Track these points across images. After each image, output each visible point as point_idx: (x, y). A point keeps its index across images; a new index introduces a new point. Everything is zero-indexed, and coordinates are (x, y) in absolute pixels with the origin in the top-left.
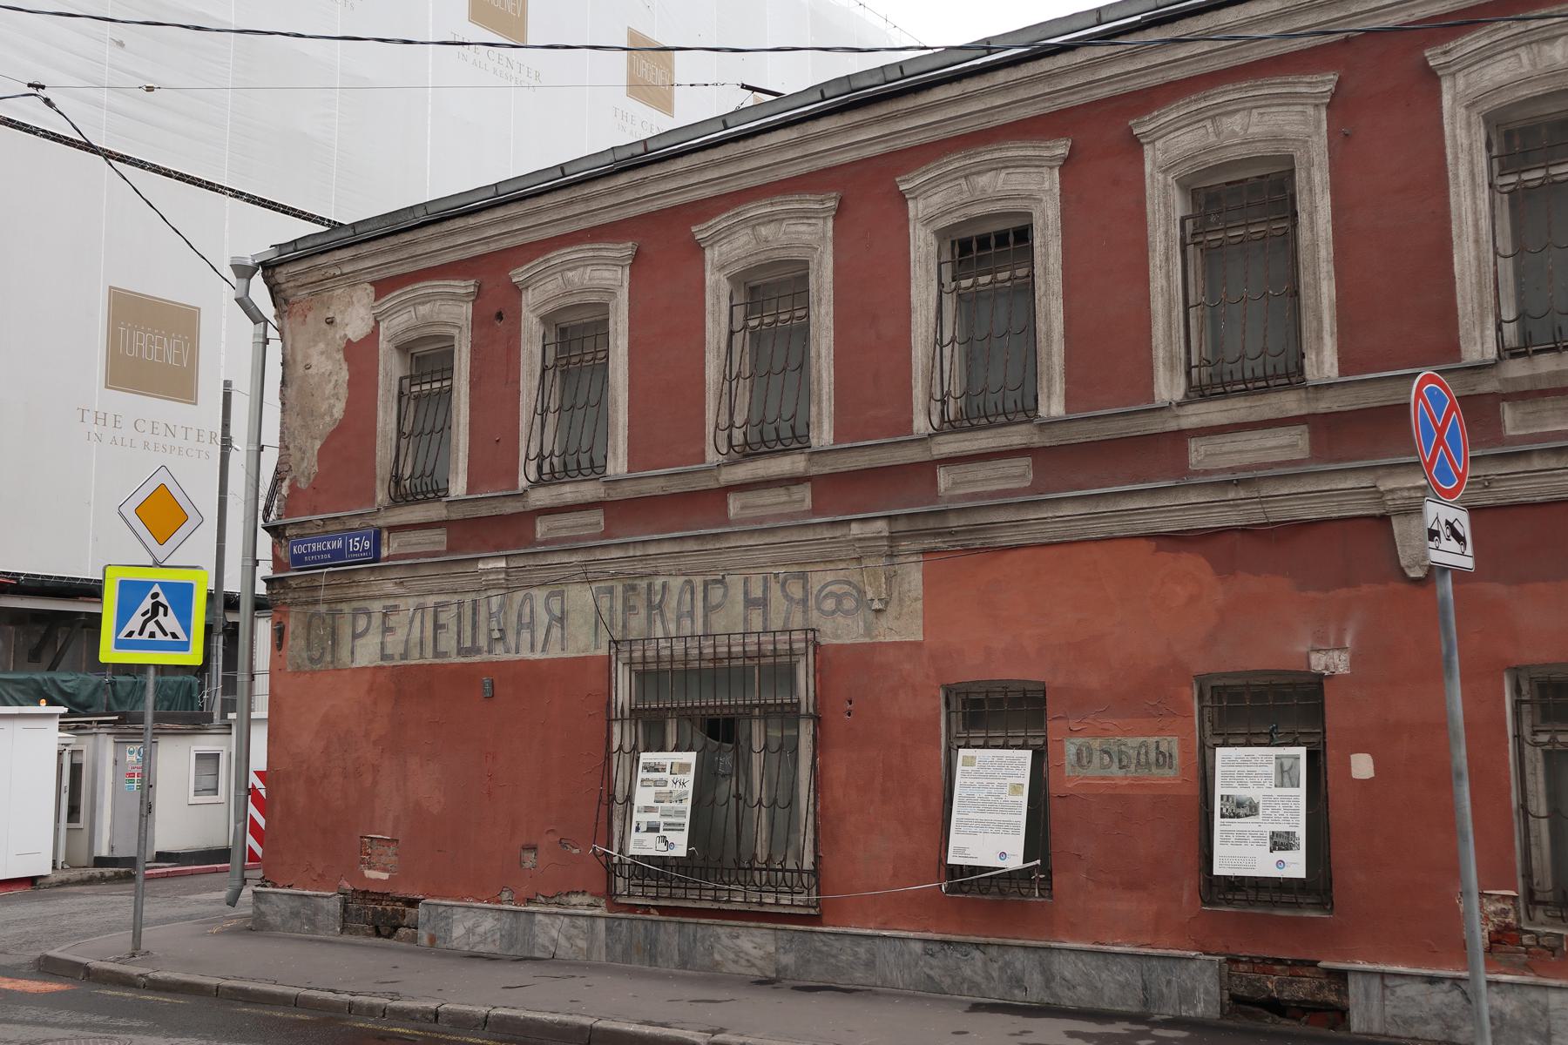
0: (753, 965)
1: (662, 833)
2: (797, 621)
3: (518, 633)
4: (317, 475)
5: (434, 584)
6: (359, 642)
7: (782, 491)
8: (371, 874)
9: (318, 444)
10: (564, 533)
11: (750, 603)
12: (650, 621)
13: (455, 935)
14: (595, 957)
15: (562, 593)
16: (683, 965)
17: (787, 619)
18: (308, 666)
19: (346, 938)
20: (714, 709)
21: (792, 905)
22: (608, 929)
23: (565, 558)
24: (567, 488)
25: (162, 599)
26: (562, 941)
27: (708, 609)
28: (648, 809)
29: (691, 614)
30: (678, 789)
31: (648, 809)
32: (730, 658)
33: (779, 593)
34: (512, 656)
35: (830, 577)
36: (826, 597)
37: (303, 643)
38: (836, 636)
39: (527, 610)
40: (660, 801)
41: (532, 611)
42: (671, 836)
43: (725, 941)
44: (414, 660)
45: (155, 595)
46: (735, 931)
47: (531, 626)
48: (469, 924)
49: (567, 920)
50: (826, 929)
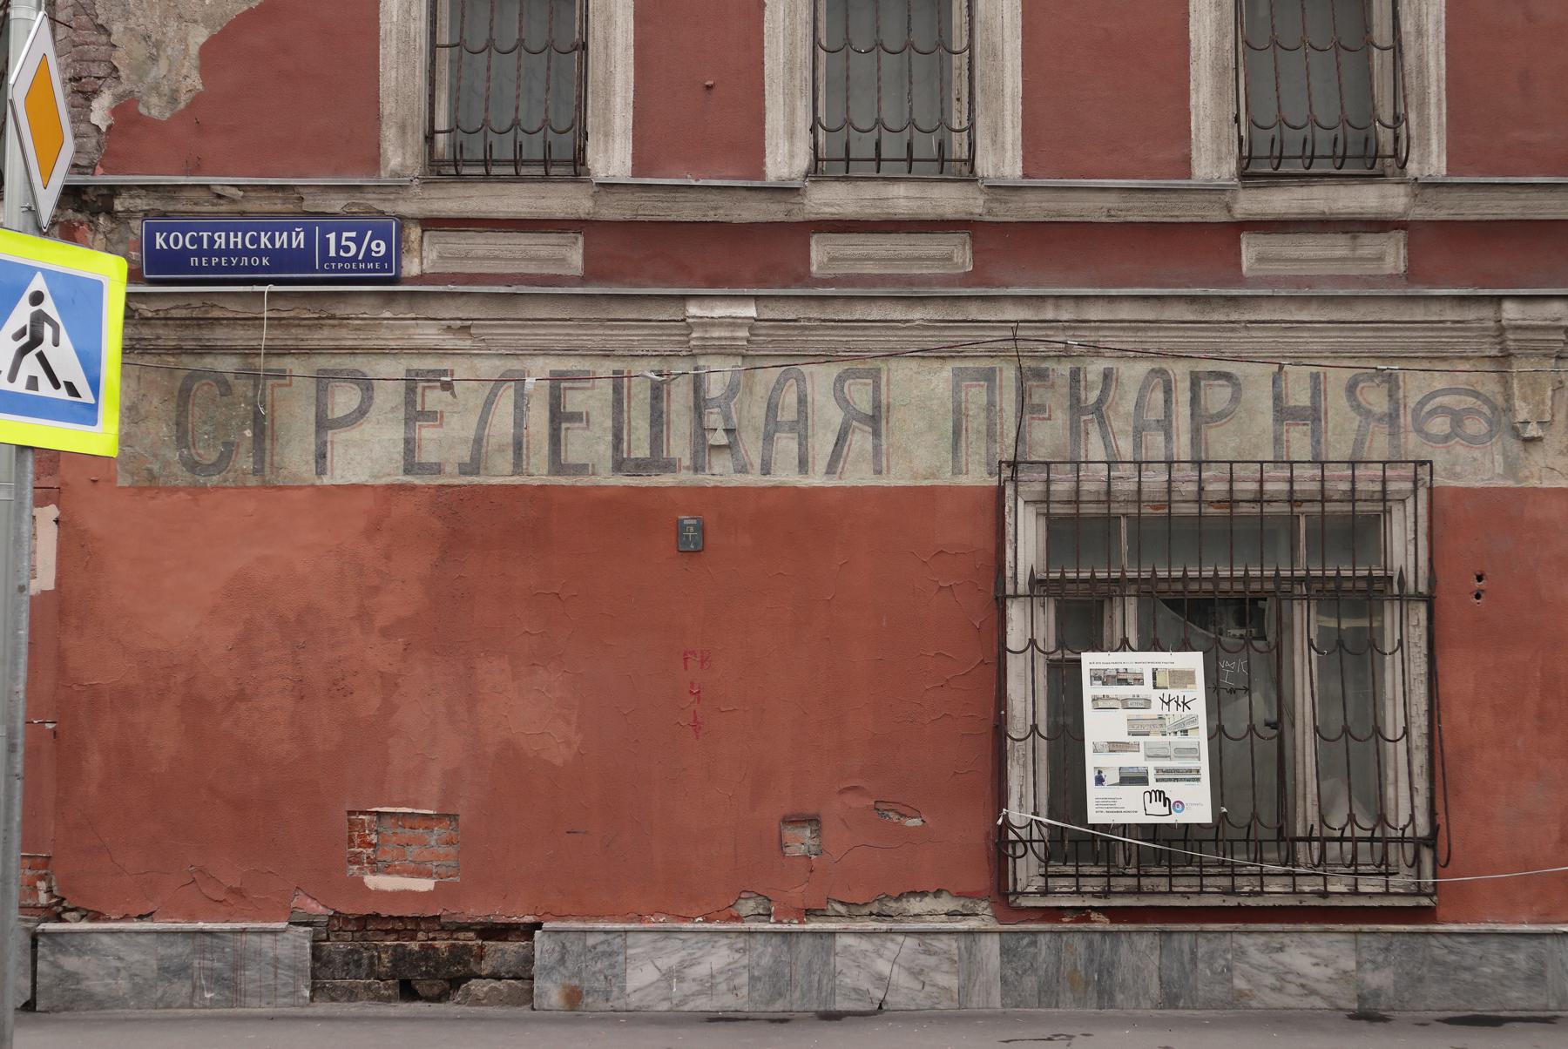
0: (1313, 992)
1: (1153, 785)
2: (1379, 446)
3: (768, 438)
4: (197, 100)
5: (543, 336)
6: (337, 437)
7: (1342, 239)
8: (374, 881)
9: (199, 36)
10: (870, 269)
11: (1283, 413)
12: (1076, 432)
13: (631, 985)
14: (976, 1002)
15: (875, 375)
16: (1170, 1000)
17: (1359, 443)
18: (183, 477)
19: (322, 1008)
20: (1224, 580)
21: (1387, 893)
22: (1005, 951)
23: (897, 313)
24: (900, 190)
25: (48, 307)
26: (901, 979)
27: (1199, 420)
28: (1115, 747)
29: (1166, 426)
30: (1174, 714)
31: (1115, 747)
32: (1324, 499)
33: (1344, 402)
34: (754, 479)
35: (1440, 382)
36: (1432, 413)
37: (165, 431)
38: (1457, 476)
39: (790, 398)
40: (1148, 734)
41: (802, 401)
42: (1173, 790)
43: (1257, 957)
44: (500, 473)
45: (37, 298)
46: (1276, 941)
47: (801, 426)
48: (670, 961)
49: (910, 942)
50: (1455, 928)
